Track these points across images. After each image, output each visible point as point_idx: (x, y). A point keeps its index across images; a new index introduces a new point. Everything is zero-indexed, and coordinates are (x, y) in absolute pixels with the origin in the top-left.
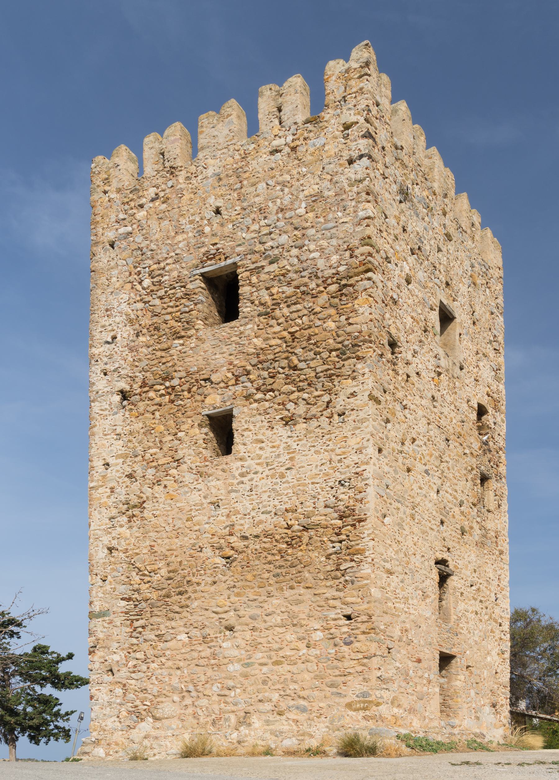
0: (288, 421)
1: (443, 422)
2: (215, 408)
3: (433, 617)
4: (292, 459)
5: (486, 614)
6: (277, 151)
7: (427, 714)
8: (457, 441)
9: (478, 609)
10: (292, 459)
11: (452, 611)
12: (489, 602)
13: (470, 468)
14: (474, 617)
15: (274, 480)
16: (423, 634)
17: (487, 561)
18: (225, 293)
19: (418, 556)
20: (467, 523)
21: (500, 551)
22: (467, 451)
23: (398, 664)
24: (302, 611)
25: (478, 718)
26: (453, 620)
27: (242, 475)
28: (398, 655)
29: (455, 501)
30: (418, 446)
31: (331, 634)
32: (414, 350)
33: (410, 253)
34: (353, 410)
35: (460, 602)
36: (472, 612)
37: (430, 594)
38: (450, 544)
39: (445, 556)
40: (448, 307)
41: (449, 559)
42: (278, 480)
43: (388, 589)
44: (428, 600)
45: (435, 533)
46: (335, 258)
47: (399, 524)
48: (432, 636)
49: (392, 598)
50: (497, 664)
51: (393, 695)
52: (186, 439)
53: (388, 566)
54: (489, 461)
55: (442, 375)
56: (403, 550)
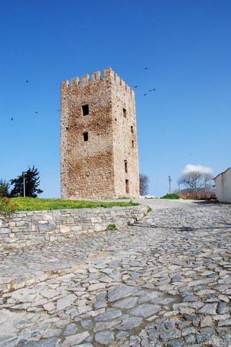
0: (98, 135)
18: (86, 110)
24: (101, 172)
33: (151, 212)
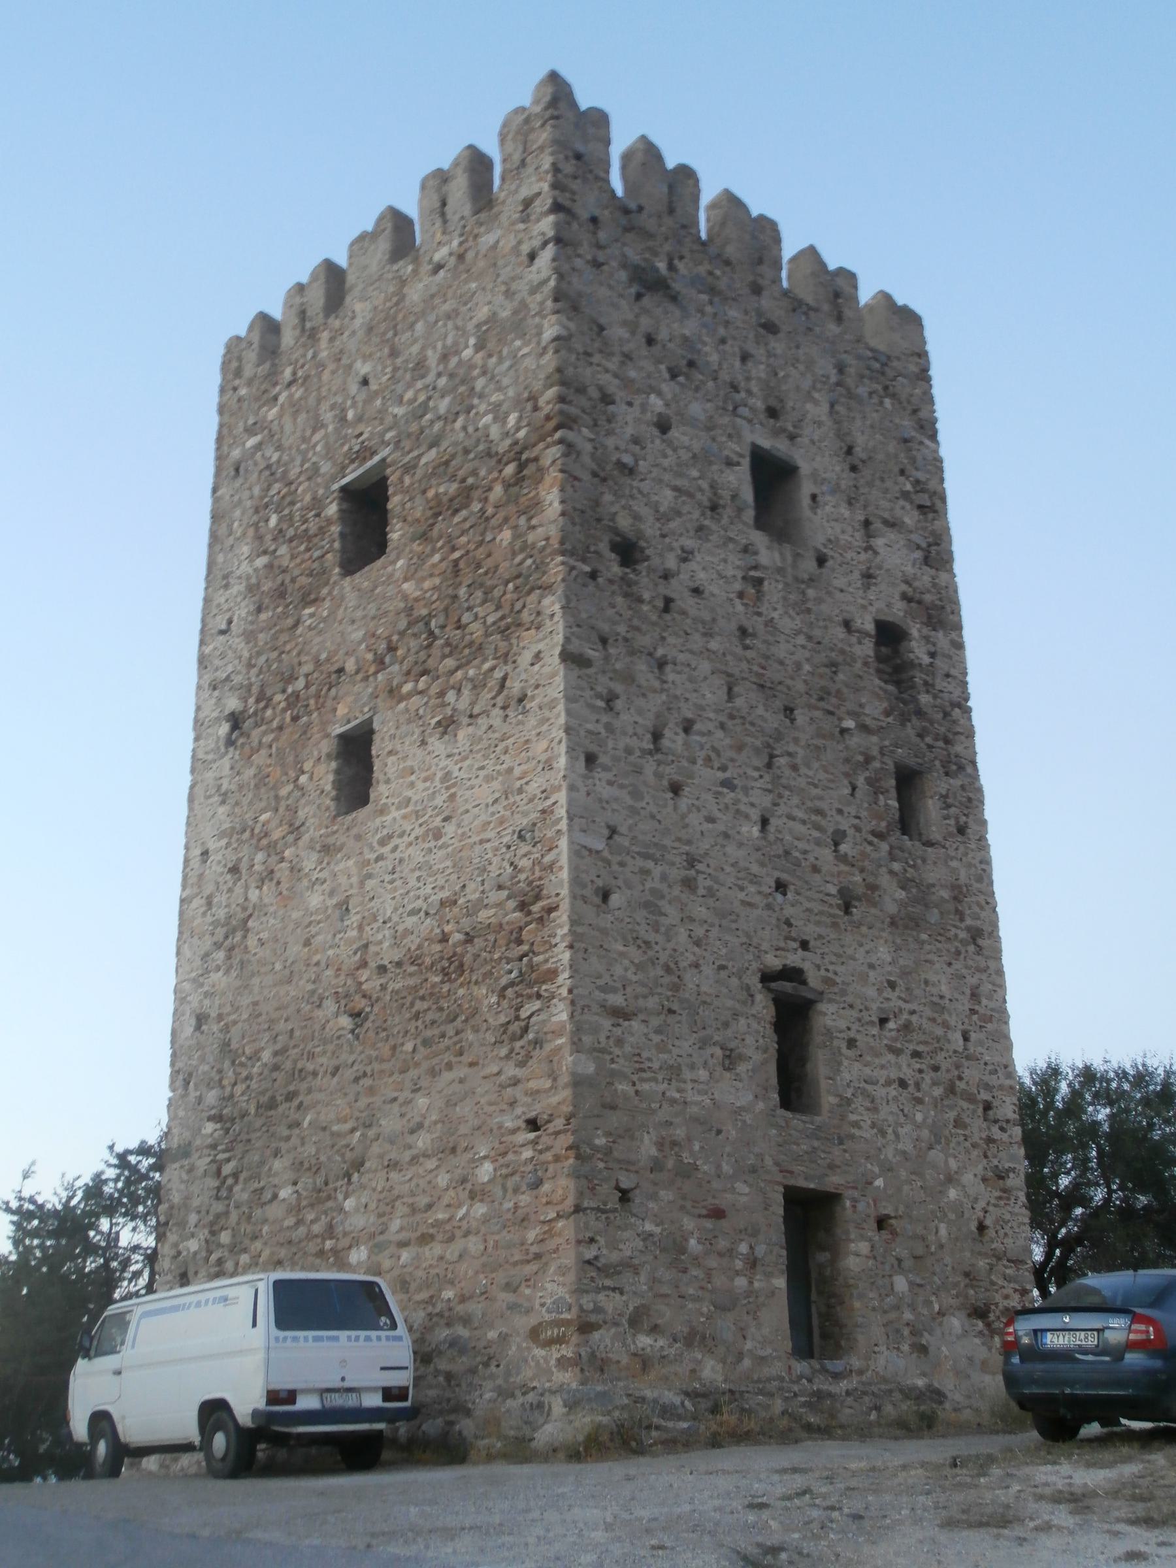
1: (774, 673)
2: (349, 722)
3: (761, 1105)
4: (453, 797)
5: (935, 1083)
6: (439, 267)
7: (749, 1345)
8: (817, 708)
9: (907, 1073)
10: (453, 797)
11: (824, 1084)
12: (943, 1054)
13: (861, 758)
14: (894, 1093)
15: (427, 845)
16: (728, 1149)
17: (929, 957)
19: (708, 970)
20: (858, 878)
21: (968, 929)
22: (849, 724)
23: (649, 1227)
25: (923, 1350)
26: (825, 1107)
27: (382, 843)
28: (651, 1205)
29: (816, 834)
30: (703, 734)
31: (508, 1166)
32: (683, 550)
34: (537, 687)
35: (846, 1063)
36: (888, 1083)
37: (749, 1052)
38: (809, 931)
39: (795, 959)
40: (774, 452)
41: (807, 966)
42: (432, 844)
43: (617, 1051)
44: (742, 1068)
45: (759, 912)
46: (512, 419)
47: (646, 905)
48: (757, 1150)
49: (628, 1071)
50: (981, 1204)
51: (638, 1302)
52: (311, 787)
53: (616, 1000)
54: (921, 736)
55: (766, 583)
56: (662, 961)
